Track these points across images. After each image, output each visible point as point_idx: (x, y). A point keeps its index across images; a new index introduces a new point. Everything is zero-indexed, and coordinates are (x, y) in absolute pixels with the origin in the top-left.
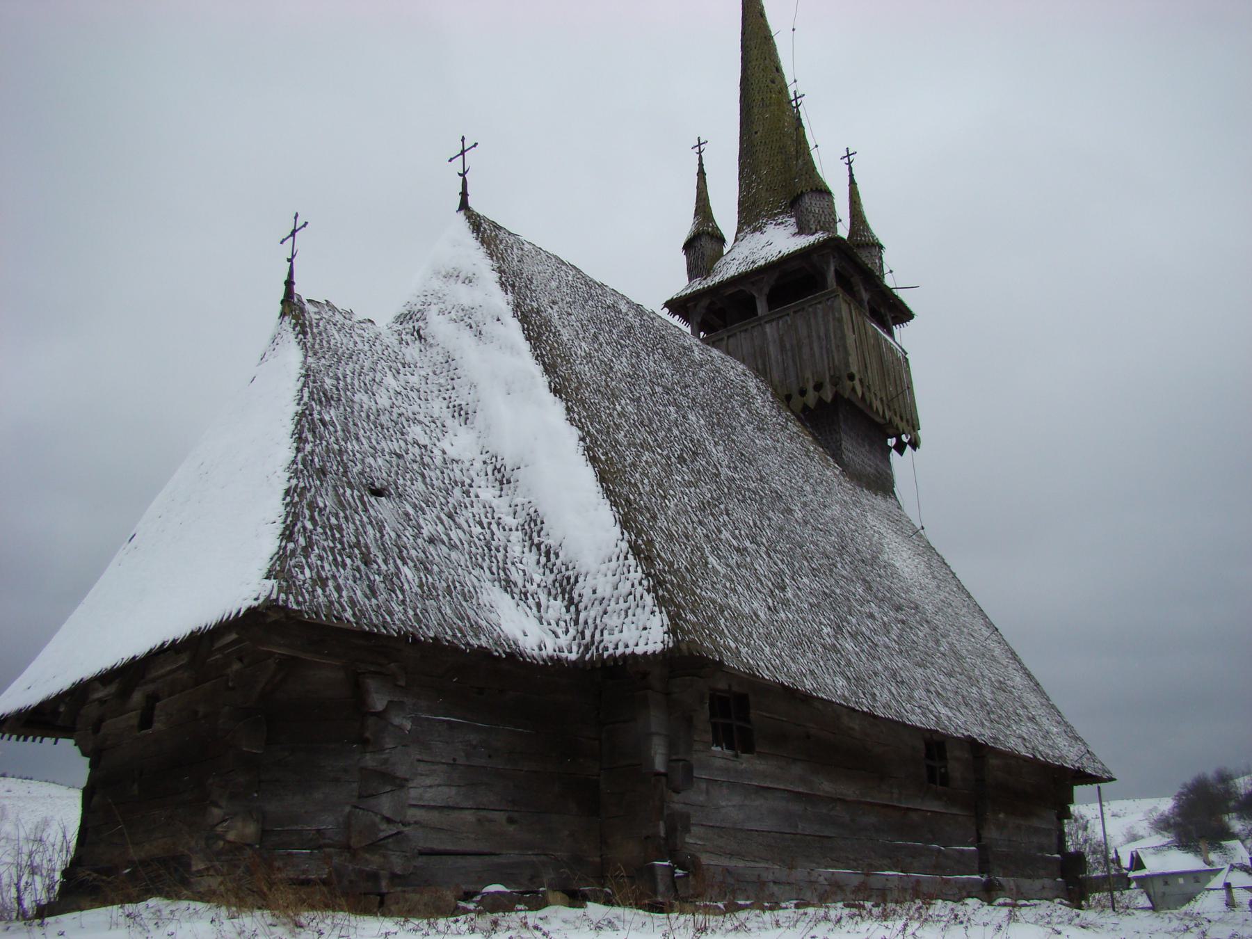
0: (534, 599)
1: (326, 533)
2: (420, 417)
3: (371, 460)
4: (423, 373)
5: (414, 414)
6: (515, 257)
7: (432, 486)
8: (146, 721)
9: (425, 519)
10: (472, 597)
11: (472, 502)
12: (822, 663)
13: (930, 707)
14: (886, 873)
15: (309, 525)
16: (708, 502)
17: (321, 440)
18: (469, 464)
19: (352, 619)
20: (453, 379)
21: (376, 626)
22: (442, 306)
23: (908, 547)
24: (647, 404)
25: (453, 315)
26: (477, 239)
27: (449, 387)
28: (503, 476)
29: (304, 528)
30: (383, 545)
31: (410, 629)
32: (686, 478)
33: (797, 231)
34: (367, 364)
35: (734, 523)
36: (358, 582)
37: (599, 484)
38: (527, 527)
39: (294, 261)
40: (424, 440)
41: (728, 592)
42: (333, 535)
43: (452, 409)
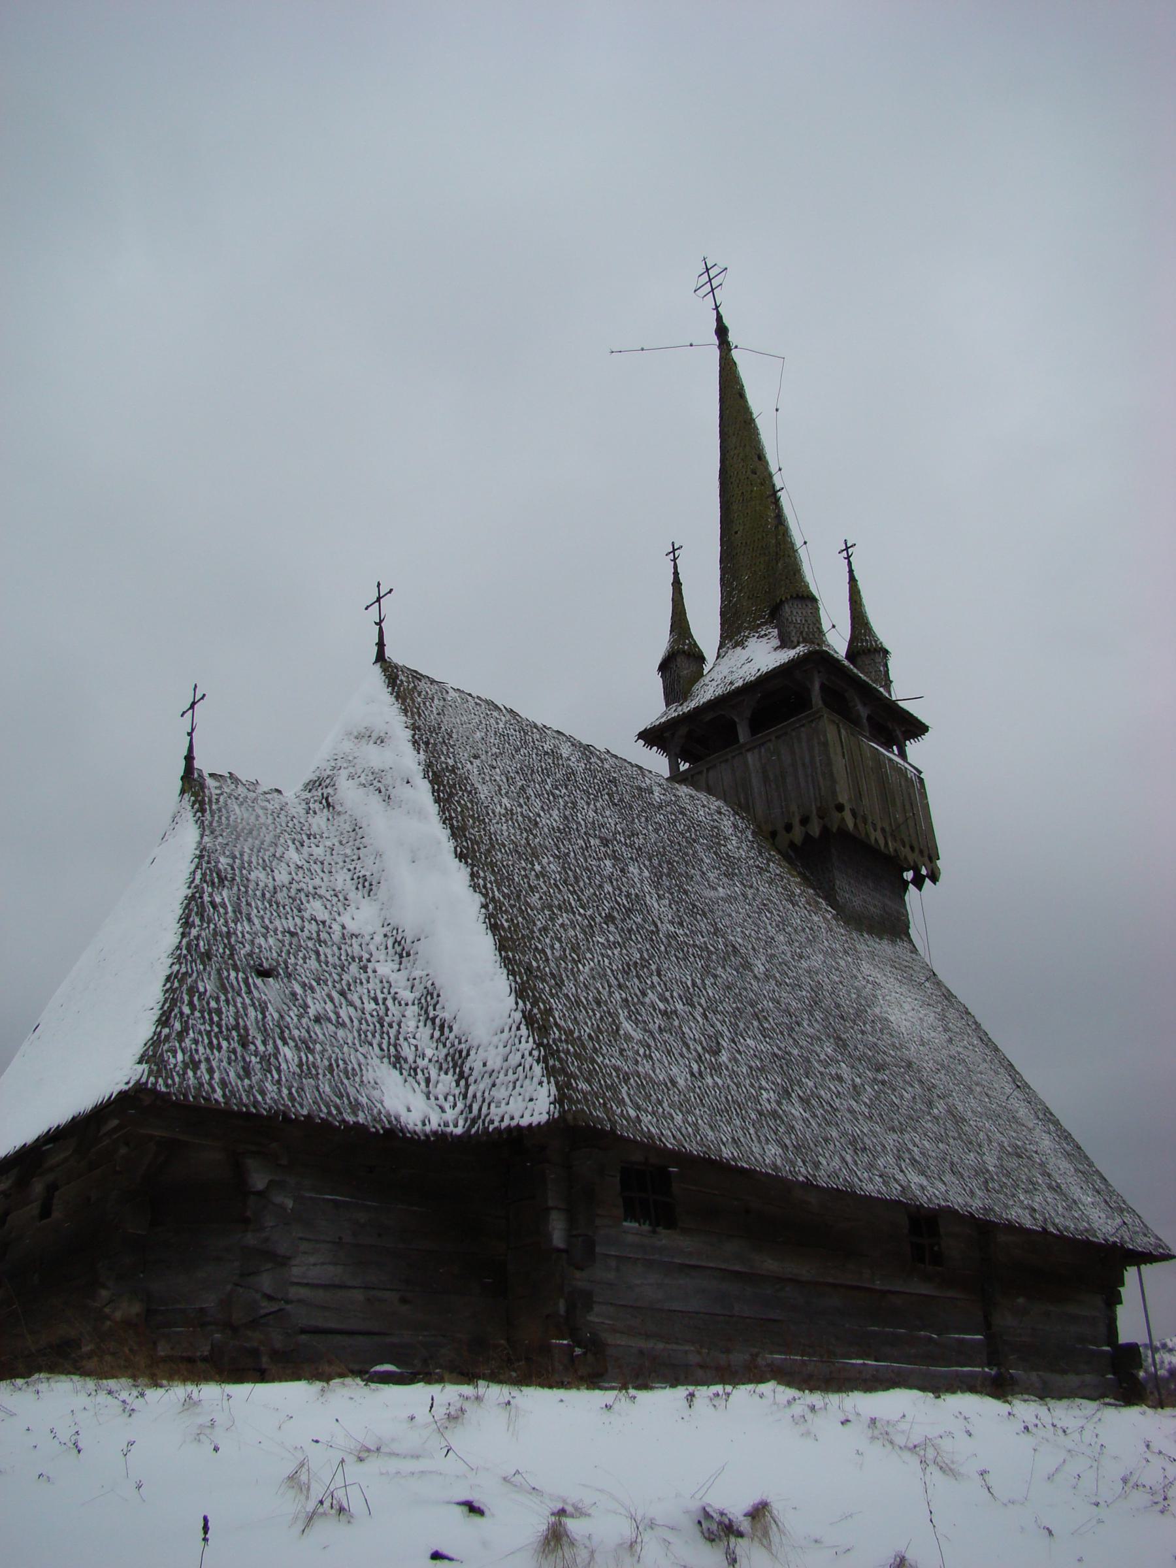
0: (423, 1074)
1: (203, 1017)
2: (322, 892)
3: (262, 941)
4: (329, 843)
5: (315, 888)
6: (434, 710)
7: (327, 963)
8: (46, 1212)
9: (314, 998)
10: (355, 1075)
11: (369, 978)
12: (752, 1131)
13: (897, 1176)
14: (853, 1361)
15: (186, 1010)
16: (636, 963)
17: (208, 923)
18: (369, 938)
19: (221, 1100)
20: (359, 849)
21: (246, 1105)
22: (352, 770)
23: (914, 996)
24: (577, 860)
25: (362, 780)
26: (392, 694)
27: (355, 857)
28: (403, 949)
29: (182, 1013)
30: (264, 1026)
31: (282, 1108)
32: (612, 939)
33: (779, 644)
34: (268, 839)
35: (665, 985)
36: (233, 1064)
37: (497, 953)
38: (423, 1001)
39: (194, 734)
40: (323, 915)
41: (639, 1059)
42: (211, 1019)
43: (356, 881)
